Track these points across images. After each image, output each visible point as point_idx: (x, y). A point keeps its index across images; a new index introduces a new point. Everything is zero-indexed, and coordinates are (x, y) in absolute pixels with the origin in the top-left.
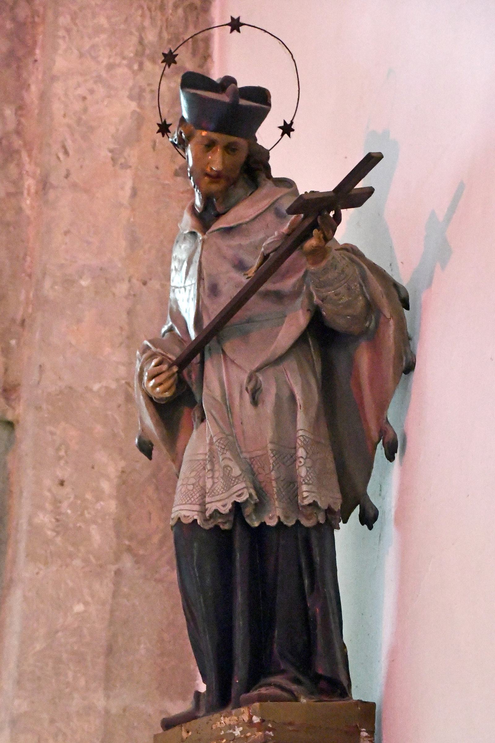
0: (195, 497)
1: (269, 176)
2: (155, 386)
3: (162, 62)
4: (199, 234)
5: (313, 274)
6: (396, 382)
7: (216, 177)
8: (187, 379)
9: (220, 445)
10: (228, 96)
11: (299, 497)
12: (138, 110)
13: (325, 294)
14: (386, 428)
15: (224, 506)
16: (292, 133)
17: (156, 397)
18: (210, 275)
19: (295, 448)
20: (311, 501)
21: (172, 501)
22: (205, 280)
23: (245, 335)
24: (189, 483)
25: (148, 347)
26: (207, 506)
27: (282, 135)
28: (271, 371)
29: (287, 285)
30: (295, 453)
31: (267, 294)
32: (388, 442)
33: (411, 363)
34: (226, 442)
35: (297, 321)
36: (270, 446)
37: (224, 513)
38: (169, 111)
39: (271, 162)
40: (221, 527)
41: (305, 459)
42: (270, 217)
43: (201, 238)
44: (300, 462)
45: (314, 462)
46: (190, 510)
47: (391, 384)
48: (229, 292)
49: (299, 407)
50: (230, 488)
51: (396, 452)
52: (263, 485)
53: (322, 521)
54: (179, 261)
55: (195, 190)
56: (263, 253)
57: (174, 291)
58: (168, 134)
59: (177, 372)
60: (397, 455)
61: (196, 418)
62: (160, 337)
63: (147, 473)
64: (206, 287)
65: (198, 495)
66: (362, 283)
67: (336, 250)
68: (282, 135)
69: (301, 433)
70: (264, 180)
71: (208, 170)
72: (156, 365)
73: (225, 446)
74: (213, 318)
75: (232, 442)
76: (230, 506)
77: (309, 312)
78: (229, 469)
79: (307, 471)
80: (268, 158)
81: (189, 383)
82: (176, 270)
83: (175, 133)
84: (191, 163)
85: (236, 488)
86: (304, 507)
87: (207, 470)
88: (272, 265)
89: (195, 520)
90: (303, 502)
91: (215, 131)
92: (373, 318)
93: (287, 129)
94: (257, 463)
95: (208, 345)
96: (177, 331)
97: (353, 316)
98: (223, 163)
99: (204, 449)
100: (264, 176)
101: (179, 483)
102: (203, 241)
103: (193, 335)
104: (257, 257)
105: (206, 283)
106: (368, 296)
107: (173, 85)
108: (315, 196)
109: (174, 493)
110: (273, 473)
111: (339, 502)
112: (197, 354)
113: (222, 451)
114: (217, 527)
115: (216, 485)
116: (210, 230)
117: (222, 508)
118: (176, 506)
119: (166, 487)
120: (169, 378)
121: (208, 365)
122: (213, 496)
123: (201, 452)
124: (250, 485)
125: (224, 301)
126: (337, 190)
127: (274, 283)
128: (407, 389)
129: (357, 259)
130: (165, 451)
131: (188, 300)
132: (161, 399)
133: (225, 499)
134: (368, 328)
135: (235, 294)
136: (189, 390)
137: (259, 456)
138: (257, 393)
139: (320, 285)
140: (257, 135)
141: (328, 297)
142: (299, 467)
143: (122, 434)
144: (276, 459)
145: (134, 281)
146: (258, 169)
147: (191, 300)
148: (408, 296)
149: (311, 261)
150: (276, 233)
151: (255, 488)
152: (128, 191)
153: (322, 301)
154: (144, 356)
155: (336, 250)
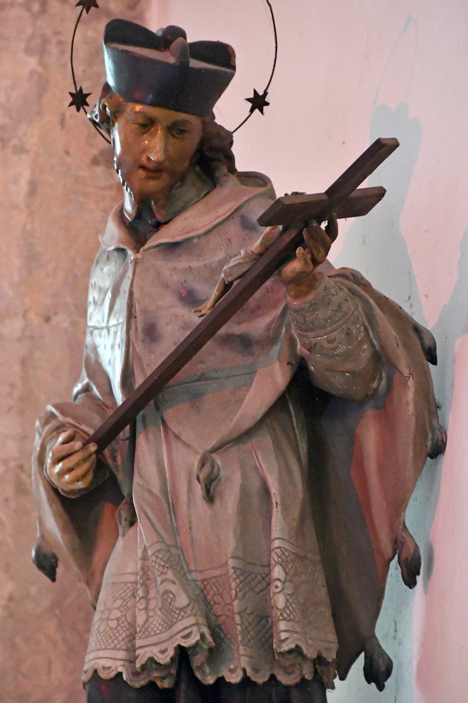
0: (120, 638)
1: (232, 170)
2: (62, 474)
3: (78, 5)
4: (130, 252)
5: (296, 311)
6: (418, 470)
7: (155, 171)
8: (110, 462)
9: (159, 561)
10: (173, 55)
11: (274, 640)
12: (39, 69)
13: (313, 341)
14: (403, 537)
15: (163, 652)
16: (265, 108)
17: (65, 489)
18: (145, 311)
19: (269, 566)
20: (293, 646)
21: (85, 643)
22: (138, 319)
23: (196, 397)
24: (112, 617)
25: (52, 416)
26: (138, 652)
27: (252, 111)
28: (234, 451)
29: (258, 326)
30: (269, 574)
31: (228, 339)
32: (407, 559)
33: (440, 443)
34: (167, 556)
35: (271, 379)
36: (231, 563)
37: (162, 662)
38: (84, 71)
39: (234, 149)
40: (159, 684)
41: (283, 583)
42: (233, 229)
43: (132, 258)
44: (277, 587)
45: (296, 588)
46: (111, 658)
47: (410, 473)
48: (173, 334)
49: (275, 506)
50: (171, 626)
51: (419, 574)
52: (221, 620)
53: (308, 677)
54: (100, 290)
55: (125, 188)
56: (223, 281)
57: (92, 333)
58: (86, 107)
59: (96, 452)
60: (419, 579)
61: (123, 519)
62: (71, 400)
63: (46, 602)
64: (140, 328)
65: (124, 635)
66: (367, 324)
67: (329, 277)
68: (252, 111)
69: (277, 543)
70: (225, 175)
71: (144, 159)
72: (65, 442)
73: (166, 562)
74: (149, 372)
75: (176, 559)
76: (171, 653)
77: (290, 366)
78: (171, 596)
79: (287, 600)
80: (231, 143)
81: (113, 469)
82: (95, 302)
83: (95, 106)
84: (118, 149)
85: (180, 626)
86: (281, 654)
87: (138, 598)
88: (236, 297)
89: (120, 674)
90: (280, 647)
91: (153, 104)
92: (384, 375)
93: (258, 102)
94: (212, 588)
95: (142, 413)
96: (96, 391)
97: (352, 373)
98: (166, 150)
99: (133, 566)
100: (225, 170)
101: (97, 617)
102: (136, 262)
103: (119, 397)
104: (214, 286)
105: (140, 323)
106: (375, 342)
107: (90, 34)
108: (298, 200)
109: (89, 631)
110: (236, 603)
111: (335, 646)
112: (125, 425)
113: (161, 569)
114: (152, 684)
115: (151, 620)
116: (146, 247)
117: (160, 655)
118: (91, 652)
119: (76, 624)
120: (85, 460)
121: (141, 441)
122: (147, 637)
123: (129, 570)
124: (202, 620)
125: (166, 347)
126: (330, 191)
127: (239, 323)
128: (433, 480)
129: (359, 289)
130: (75, 568)
131: (113, 347)
132: (72, 492)
133: (167, 640)
134: (376, 390)
135: (182, 340)
136: (113, 478)
137: (215, 577)
138: (214, 484)
139: (306, 328)
140: (215, 110)
141: (318, 347)
142: (275, 594)
143: (10, 541)
144: (241, 582)
145: (32, 316)
146: (218, 160)
147: (117, 347)
148: (434, 341)
149: (293, 293)
150: (242, 252)
151: (210, 627)
152: (23, 187)
153: (309, 350)
154: (47, 428)
155: (329, 277)
